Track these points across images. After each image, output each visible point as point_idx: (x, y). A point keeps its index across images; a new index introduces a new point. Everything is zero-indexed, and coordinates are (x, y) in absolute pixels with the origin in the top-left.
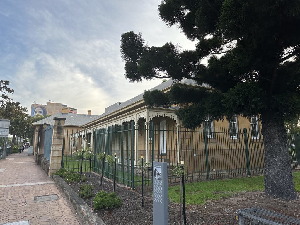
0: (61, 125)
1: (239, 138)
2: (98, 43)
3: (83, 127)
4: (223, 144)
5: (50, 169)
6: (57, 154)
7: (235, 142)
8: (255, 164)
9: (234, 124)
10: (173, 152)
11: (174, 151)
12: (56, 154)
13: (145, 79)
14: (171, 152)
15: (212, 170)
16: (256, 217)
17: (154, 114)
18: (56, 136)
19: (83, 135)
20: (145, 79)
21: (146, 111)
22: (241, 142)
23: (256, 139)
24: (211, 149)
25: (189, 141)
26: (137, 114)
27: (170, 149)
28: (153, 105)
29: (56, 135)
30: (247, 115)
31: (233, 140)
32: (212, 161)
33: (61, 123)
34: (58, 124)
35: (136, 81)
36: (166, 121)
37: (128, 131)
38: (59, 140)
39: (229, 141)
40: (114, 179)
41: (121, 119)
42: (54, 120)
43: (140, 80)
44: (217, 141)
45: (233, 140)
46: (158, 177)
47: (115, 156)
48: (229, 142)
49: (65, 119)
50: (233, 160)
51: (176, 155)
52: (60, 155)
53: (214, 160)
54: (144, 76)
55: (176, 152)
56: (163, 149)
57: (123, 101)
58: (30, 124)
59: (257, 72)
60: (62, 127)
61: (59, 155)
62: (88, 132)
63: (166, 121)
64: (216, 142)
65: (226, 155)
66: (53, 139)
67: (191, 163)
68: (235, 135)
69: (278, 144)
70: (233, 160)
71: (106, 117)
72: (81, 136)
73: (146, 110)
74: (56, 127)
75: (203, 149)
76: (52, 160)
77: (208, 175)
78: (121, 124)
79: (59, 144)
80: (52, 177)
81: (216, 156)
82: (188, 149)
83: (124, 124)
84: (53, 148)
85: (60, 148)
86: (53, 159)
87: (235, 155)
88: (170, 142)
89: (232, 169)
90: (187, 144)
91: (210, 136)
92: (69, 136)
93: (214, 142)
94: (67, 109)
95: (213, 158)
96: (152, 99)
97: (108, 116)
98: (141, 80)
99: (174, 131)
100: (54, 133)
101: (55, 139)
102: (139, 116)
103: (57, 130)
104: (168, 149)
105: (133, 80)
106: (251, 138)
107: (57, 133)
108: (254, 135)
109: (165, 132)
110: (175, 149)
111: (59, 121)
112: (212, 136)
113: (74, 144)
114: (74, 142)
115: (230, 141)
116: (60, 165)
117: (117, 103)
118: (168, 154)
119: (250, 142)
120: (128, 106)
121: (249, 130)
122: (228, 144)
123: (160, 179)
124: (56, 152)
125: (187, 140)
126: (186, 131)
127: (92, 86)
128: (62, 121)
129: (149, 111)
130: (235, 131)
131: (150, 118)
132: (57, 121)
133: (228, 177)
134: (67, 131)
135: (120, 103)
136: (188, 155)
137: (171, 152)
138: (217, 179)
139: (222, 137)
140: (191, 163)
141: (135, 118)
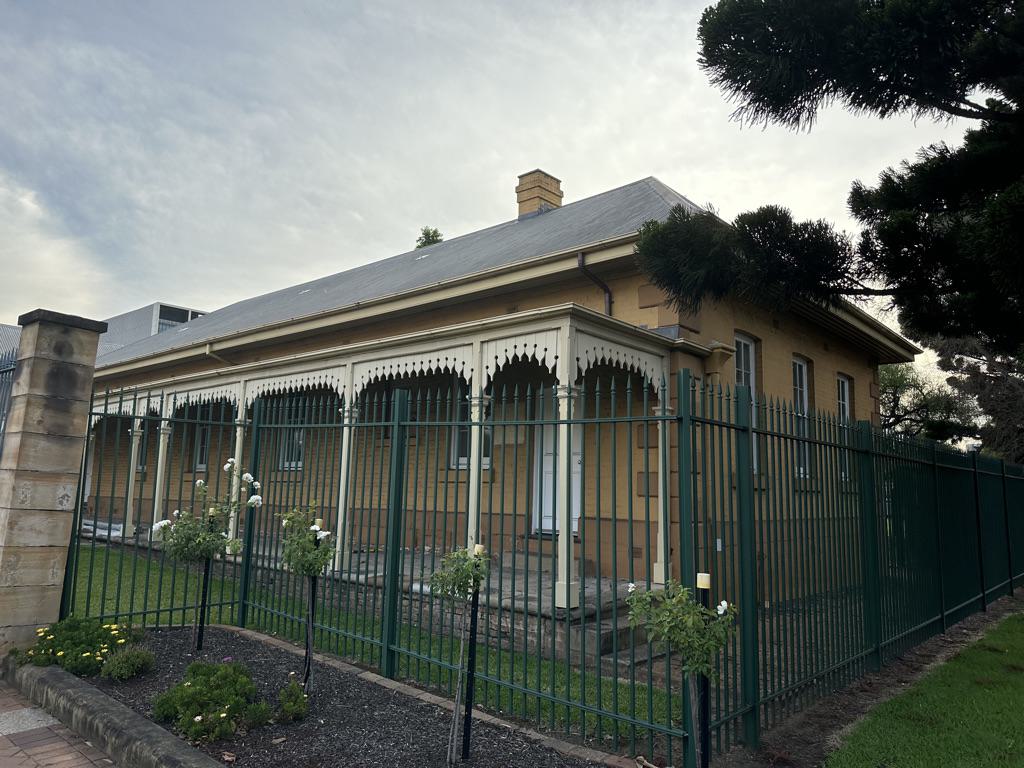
0: (76, 358)
2: (78, 55)
10: (420, 516)
11: (627, 525)
14: (607, 531)
18: (40, 422)
26: (482, 342)
27: (496, 509)
29: (37, 414)
33: (75, 345)
34: (59, 349)
37: (294, 429)
38: (54, 448)
40: (459, 689)
41: (355, 359)
55: (333, 512)
56: (548, 510)
57: (206, 300)
60: (79, 371)
71: (206, 350)
73: (566, 324)
74: (45, 369)
85: (61, 492)
86: (12, 559)
88: (607, 482)
97: (217, 347)
100: (28, 404)
101: (32, 441)
103: (48, 387)
104: (591, 512)
107: (46, 407)
110: (334, 505)
111: (66, 332)
119: (726, 484)
120: (359, 307)
124: (37, 521)
128: (84, 336)
129: (578, 331)
132: (54, 333)
135: (173, 315)
137: (607, 531)
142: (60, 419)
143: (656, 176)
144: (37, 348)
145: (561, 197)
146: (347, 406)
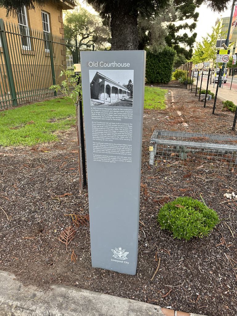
4: (16, 56)
7: (33, 55)
8: (17, 81)
16: (181, 142)
22: (35, 55)
23: (26, 49)
28: (221, 10)
30: (146, 32)
32: (4, 81)
39: (45, 55)
44: (33, 54)
48: (22, 54)
50: (28, 78)
65: (21, 73)
70: (28, 78)
77: (213, 111)
87: (30, 72)
89: (28, 90)
115: (23, 53)
122: (21, 57)
133: (36, 100)
138: (25, 103)
139: (14, 47)
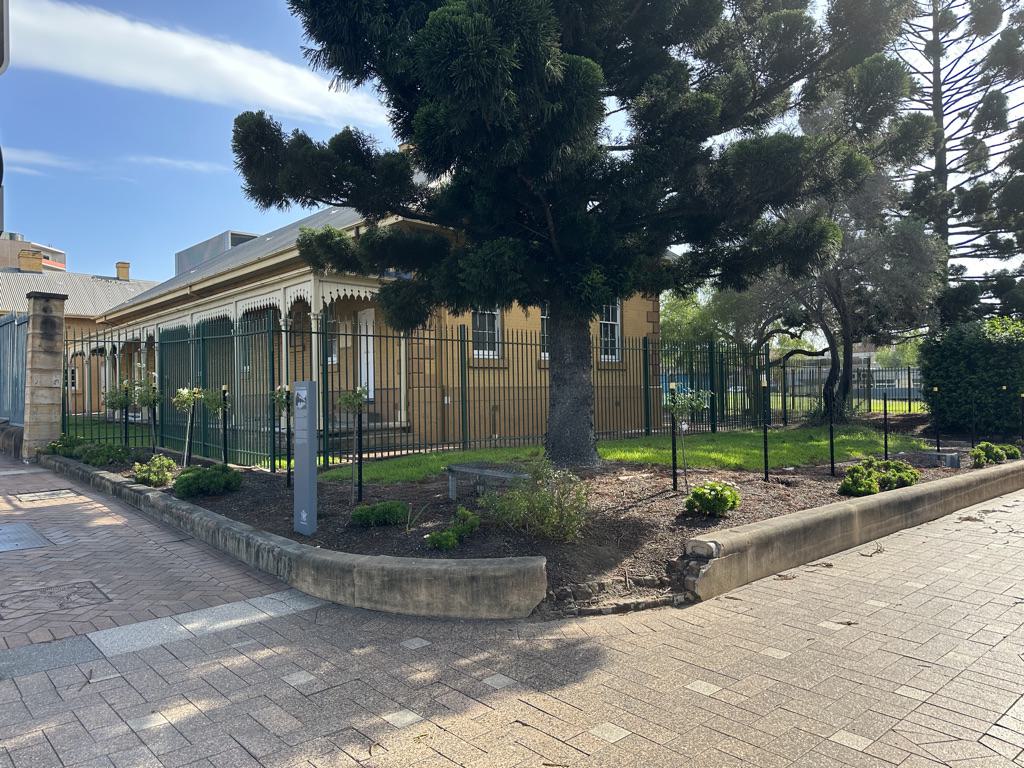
0: (54, 314)
1: (503, 358)
3: (103, 320)
5: (25, 437)
6: (46, 397)
9: (613, 326)
10: (391, 392)
12: (42, 396)
13: (299, 205)
15: (491, 437)
17: (334, 291)
19: (108, 347)
20: (299, 205)
21: (313, 281)
24: (482, 385)
25: (433, 365)
29: (38, 342)
31: (486, 362)
35: (273, 208)
36: (373, 309)
38: (49, 358)
41: (236, 299)
42: (29, 296)
43: (284, 203)
45: (486, 362)
46: (301, 405)
47: (225, 392)
49: (65, 297)
51: (397, 401)
52: (56, 399)
53: (497, 414)
54: (296, 197)
55: (397, 392)
58: (805, 377)
59: (592, 201)
60: (56, 320)
61: (52, 399)
62: (130, 336)
63: (373, 309)
64: (504, 368)
66: (29, 355)
67: (434, 420)
68: (613, 353)
69: (570, 364)
71: (187, 291)
72: (102, 351)
73: (311, 277)
74: (39, 320)
75: (456, 385)
76: (33, 413)
78: (240, 314)
79: (52, 367)
80: (35, 460)
81: (502, 402)
82: (428, 384)
83: (247, 314)
84: (32, 382)
85: (54, 379)
90: (427, 372)
91: (491, 353)
92: (74, 346)
93: (494, 368)
94: (37, 256)
95: (495, 407)
96: (319, 252)
97: (195, 288)
98: (288, 203)
99: (387, 337)
100: (33, 337)
101: (36, 355)
102: (293, 294)
103: (41, 329)
105: (268, 205)
106: (538, 357)
107: (42, 338)
108: (606, 353)
109: (370, 339)
110: (397, 386)
112: (496, 353)
113: (73, 378)
114: (73, 372)
116: (59, 426)
117: (222, 237)
118: (378, 400)
120: (260, 260)
121: (524, 335)
123: (304, 407)
125: (427, 361)
126: (424, 339)
127: (162, 235)
128: (57, 303)
130: (613, 343)
131: (324, 303)
132: (42, 302)
134: (68, 332)
135: (238, 239)
136: (428, 399)
140: (434, 420)
141: (281, 296)
142: (50, 344)
143: (177, 252)
144: (34, 310)
145: (128, 268)
146: (283, 316)
